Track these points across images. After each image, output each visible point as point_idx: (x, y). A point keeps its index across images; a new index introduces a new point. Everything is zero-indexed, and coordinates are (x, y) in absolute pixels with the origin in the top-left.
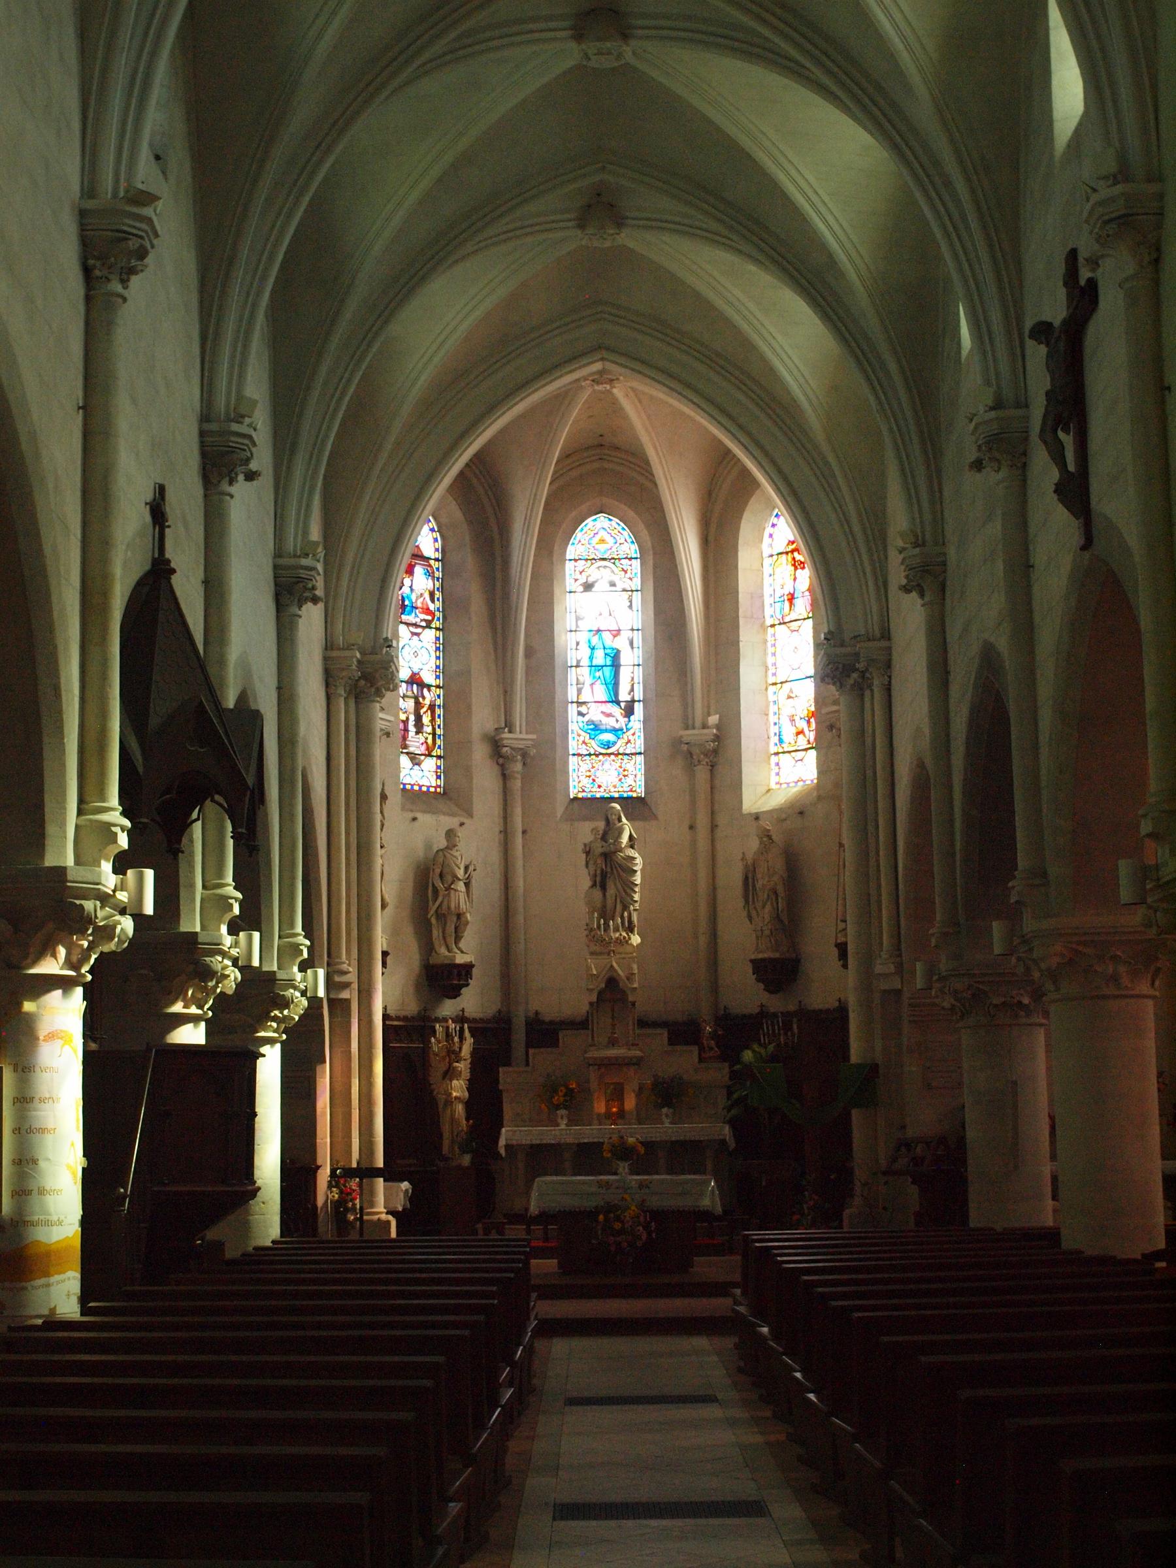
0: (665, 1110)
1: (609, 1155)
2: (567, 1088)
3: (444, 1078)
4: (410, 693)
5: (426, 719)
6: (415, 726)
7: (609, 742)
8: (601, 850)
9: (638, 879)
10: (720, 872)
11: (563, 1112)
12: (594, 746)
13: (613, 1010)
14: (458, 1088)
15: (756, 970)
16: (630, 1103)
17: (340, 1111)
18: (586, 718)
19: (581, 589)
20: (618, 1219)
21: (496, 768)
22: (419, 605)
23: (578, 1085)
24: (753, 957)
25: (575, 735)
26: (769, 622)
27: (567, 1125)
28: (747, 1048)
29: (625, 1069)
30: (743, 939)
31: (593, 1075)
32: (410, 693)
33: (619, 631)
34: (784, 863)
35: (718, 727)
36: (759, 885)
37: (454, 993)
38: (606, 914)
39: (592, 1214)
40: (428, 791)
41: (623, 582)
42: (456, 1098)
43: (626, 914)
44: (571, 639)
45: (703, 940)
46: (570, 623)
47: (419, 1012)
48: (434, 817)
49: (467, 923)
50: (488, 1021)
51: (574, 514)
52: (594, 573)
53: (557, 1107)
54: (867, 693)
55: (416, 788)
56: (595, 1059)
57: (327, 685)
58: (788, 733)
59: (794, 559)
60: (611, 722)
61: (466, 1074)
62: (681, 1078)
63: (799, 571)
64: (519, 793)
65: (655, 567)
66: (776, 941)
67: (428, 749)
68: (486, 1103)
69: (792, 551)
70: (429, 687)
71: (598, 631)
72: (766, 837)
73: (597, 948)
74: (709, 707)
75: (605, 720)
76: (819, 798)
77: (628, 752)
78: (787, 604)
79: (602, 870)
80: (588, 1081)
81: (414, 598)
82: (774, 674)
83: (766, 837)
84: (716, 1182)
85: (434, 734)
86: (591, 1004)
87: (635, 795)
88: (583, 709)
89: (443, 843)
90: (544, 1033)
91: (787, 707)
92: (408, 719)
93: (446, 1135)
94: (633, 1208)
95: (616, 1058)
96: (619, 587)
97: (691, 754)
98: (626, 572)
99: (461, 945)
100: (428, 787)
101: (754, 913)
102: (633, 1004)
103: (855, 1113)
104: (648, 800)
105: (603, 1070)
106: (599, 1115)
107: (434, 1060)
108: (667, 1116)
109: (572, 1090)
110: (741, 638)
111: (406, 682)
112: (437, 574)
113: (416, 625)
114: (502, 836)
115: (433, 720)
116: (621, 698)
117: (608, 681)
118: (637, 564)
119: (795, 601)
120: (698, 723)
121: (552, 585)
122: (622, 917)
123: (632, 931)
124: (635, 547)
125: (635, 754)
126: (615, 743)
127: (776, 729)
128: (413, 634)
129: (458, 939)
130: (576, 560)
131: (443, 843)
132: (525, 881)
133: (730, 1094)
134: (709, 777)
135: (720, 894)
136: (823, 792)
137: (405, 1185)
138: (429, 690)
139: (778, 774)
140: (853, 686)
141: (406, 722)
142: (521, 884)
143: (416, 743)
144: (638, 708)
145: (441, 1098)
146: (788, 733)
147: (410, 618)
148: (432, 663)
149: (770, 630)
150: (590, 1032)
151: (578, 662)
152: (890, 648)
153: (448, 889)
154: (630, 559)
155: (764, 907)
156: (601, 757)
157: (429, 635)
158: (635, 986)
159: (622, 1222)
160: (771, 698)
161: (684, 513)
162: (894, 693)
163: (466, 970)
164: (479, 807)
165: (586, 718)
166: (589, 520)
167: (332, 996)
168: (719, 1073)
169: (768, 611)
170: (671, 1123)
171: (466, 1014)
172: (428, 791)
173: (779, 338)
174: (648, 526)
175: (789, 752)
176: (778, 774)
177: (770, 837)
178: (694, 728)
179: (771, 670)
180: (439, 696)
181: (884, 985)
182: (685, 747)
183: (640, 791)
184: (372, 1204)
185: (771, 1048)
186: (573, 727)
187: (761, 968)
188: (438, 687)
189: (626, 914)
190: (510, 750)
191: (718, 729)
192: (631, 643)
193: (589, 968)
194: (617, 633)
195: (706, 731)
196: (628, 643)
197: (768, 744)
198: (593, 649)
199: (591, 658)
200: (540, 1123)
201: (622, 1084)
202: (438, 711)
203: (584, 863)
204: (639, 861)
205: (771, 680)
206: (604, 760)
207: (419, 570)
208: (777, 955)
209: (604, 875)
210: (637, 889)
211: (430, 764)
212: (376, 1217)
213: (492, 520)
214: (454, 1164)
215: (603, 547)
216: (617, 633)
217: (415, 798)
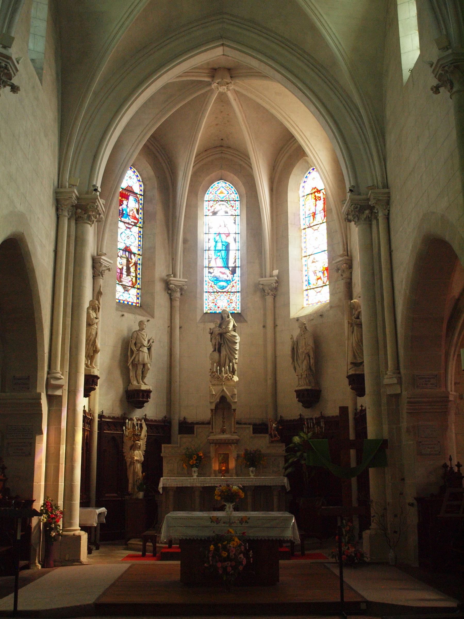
0: (251, 469)
1: (219, 498)
2: (197, 455)
3: (131, 449)
4: (124, 256)
5: (132, 269)
6: (126, 272)
7: (223, 286)
8: (219, 332)
9: (237, 347)
10: (279, 347)
11: (195, 469)
12: (216, 288)
13: (223, 414)
14: (138, 455)
15: (298, 396)
16: (232, 464)
17: (52, 465)
18: (212, 275)
19: (211, 214)
20: (225, 548)
21: (167, 295)
22: (131, 214)
23: (204, 454)
24: (297, 389)
25: (207, 283)
26: (302, 228)
27: (197, 476)
28: (297, 435)
29: (230, 446)
30: (291, 380)
31: (212, 449)
32: (124, 256)
33: (229, 234)
34: (313, 343)
35: (278, 276)
36: (300, 351)
37: (140, 405)
38: (220, 364)
39: (206, 542)
40: (132, 305)
41: (231, 212)
42: (136, 460)
43: (231, 364)
44: (206, 237)
45: (270, 382)
46: (206, 230)
47: (122, 415)
48: (133, 316)
49: (149, 369)
50: (159, 421)
51: (208, 178)
52: (217, 207)
53: (192, 466)
54: (374, 222)
55: (126, 302)
56: (213, 440)
57: (57, 209)
58: (313, 279)
59: (315, 196)
60: (225, 277)
61: (143, 447)
62: (260, 451)
63: (318, 202)
64: (178, 309)
65: (247, 202)
66: (309, 381)
67: (133, 284)
68: (153, 465)
69: (314, 193)
70: (134, 254)
71: (219, 234)
72: (304, 328)
73: (216, 382)
74: (273, 268)
75: (222, 276)
76: (331, 307)
77: (233, 291)
78: (312, 217)
79: (219, 343)
80: (209, 453)
81: (128, 210)
82: (305, 252)
83: (304, 328)
84: (296, 519)
85: (136, 277)
86: (212, 410)
87: (236, 312)
88: (211, 270)
89: (138, 328)
90: (187, 428)
91: (312, 267)
92: (122, 268)
93: (131, 481)
94: (236, 539)
95: (225, 440)
96: (229, 214)
97: (264, 290)
98: (233, 207)
99: (145, 380)
100: (132, 303)
101: (296, 365)
102: (235, 410)
103: (371, 470)
104: (242, 314)
105: (217, 446)
106: (215, 471)
107: (125, 439)
108: (252, 472)
109: (201, 456)
110: (289, 234)
111: (123, 250)
112: (141, 202)
113: (128, 224)
114: (169, 328)
115: (136, 270)
116: (230, 265)
117: (224, 257)
118: (238, 203)
119: (316, 216)
120: (268, 274)
121: (197, 210)
122: (229, 366)
123: (234, 374)
124: (237, 196)
125: (236, 292)
126: (226, 287)
127: (306, 278)
128: (127, 228)
129: (143, 377)
130: (209, 201)
131: (138, 328)
132: (180, 352)
133: (286, 461)
134: (273, 301)
135: (278, 359)
136: (331, 305)
137: (103, 509)
138: (135, 256)
139: (307, 300)
140: (365, 219)
141: (121, 269)
142: (178, 353)
143: (126, 280)
144: (238, 271)
145: (128, 460)
146: (313, 279)
147: (126, 220)
148: (137, 243)
149: (303, 231)
150: (211, 426)
151: (209, 248)
152: (389, 193)
153: (138, 350)
154: (235, 201)
155: (302, 363)
156: (219, 293)
157: (135, 230)
158: (236, 400)
159: (228, 551)
160: (304, 263)
161: (262, 174)
162: (391, 219)
163: (147, 393)
164: (157, 313)
165: (212, 275)
166: (216, 183)
167: (50, 393)
168: (281, 449)
169: (302, 222)
170: (254, 476)
171: (147, 417)
172: (132, 305)
173: (325, 17)
174: (244, 184)
175: (313, 288)
176: (307, 300)
177: (305, 327)
178: (265, 277)
179: (304, 250)
180: (139, 259)
181: (390, 391)
182: (261, 287)
183: (238, 310)
184: (71, 524)
185: (310, 434)
186: (206, 279)
187: (300, 394)
188: (139, 255)
189: (231, 364)
190: (174, 288)
191: (278, 277)
192: (235, 240)
193: (211, 391)
194: (228, 235)
195: (272, 278)
196: (233, 239)
197: (302, 285)
198: (216, 242)
199: (215, 247)
200: (183, 475)
201: (228, 454)
202: (138, 266)
203: (210, 339)
204: (238, 337)
205: (304, 254)
206: (221, 294)
207: (131, 198)
208: (309, 388)
209: (220, 345)
210: (237, 352)
211: (134, 292)
212: (72, 533)
213: (169, 178)
214: (134, 497)
215: (222, 195)
216: (228, 235)
217: (123, 306)
